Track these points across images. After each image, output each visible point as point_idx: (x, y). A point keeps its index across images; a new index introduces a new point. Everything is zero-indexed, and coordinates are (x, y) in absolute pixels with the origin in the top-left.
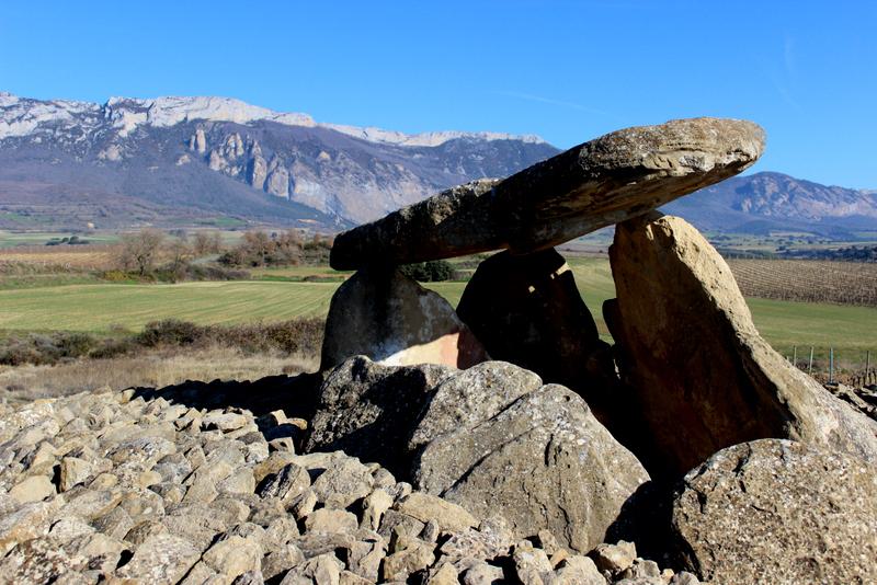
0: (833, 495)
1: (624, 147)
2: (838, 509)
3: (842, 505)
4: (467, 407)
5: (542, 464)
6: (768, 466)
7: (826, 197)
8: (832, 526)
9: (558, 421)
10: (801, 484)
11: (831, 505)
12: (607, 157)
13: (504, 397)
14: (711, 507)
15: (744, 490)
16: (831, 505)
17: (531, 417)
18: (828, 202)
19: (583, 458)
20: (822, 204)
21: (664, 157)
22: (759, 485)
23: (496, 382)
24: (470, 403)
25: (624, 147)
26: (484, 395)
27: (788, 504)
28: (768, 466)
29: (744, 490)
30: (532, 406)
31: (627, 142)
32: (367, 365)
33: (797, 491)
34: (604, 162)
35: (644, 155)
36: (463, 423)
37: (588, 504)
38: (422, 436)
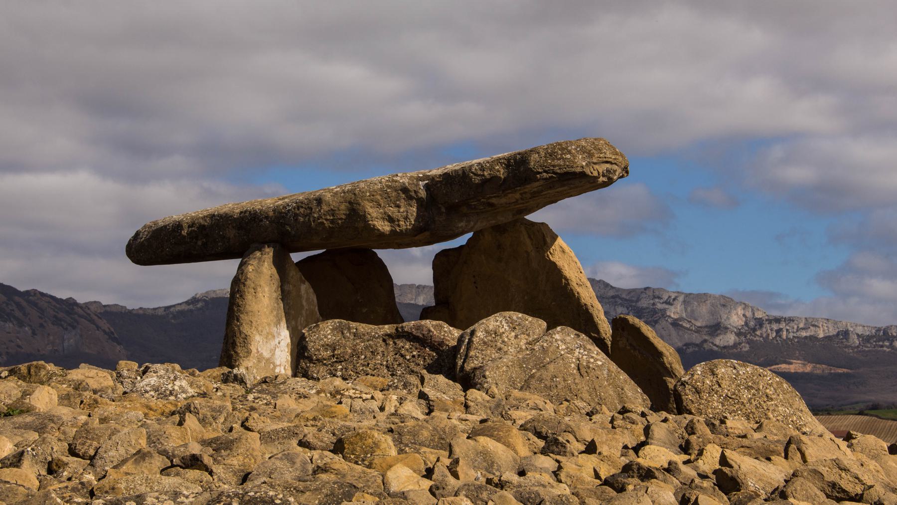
0: (768, 391)
1: (568, 156)
2: (772, 399)
3: (773, 397)
4: (503, 342)
5: (578, 376)
6: (729, 372)
7: (17, 313)
8: (771, 408)
9: (578, 350)
10: (750, 384)
11: (767, 396)
12: (556, 162)
13: (528, 335)
14: (705, 396)
15: (720, 386)
16: (767, 396)
17: (558, 347)
18: (21, 324)
19: (605, 372)
20: (9, 326)
21: (596, 167)
22: (728, 383)
23: (519, 325)
24: (506, 340)
25: (568, 156)
26: (513, 334)
27: (746, 395)
28: (729, 372)
29: (720, 386)
30: (556, 340)
31: (570, 152)
32: (127, 367)
33: (749, 388)
34: (554, 166)
35: (584, 164)
36: (506, 353)
37: (616, 401)
38: (476, 362)
